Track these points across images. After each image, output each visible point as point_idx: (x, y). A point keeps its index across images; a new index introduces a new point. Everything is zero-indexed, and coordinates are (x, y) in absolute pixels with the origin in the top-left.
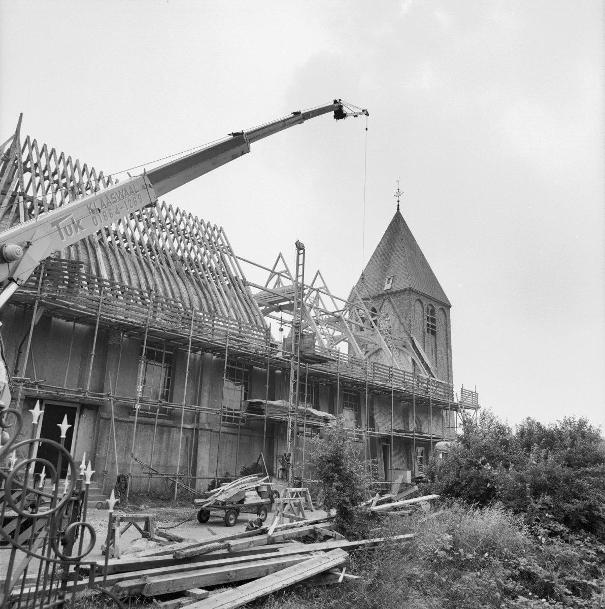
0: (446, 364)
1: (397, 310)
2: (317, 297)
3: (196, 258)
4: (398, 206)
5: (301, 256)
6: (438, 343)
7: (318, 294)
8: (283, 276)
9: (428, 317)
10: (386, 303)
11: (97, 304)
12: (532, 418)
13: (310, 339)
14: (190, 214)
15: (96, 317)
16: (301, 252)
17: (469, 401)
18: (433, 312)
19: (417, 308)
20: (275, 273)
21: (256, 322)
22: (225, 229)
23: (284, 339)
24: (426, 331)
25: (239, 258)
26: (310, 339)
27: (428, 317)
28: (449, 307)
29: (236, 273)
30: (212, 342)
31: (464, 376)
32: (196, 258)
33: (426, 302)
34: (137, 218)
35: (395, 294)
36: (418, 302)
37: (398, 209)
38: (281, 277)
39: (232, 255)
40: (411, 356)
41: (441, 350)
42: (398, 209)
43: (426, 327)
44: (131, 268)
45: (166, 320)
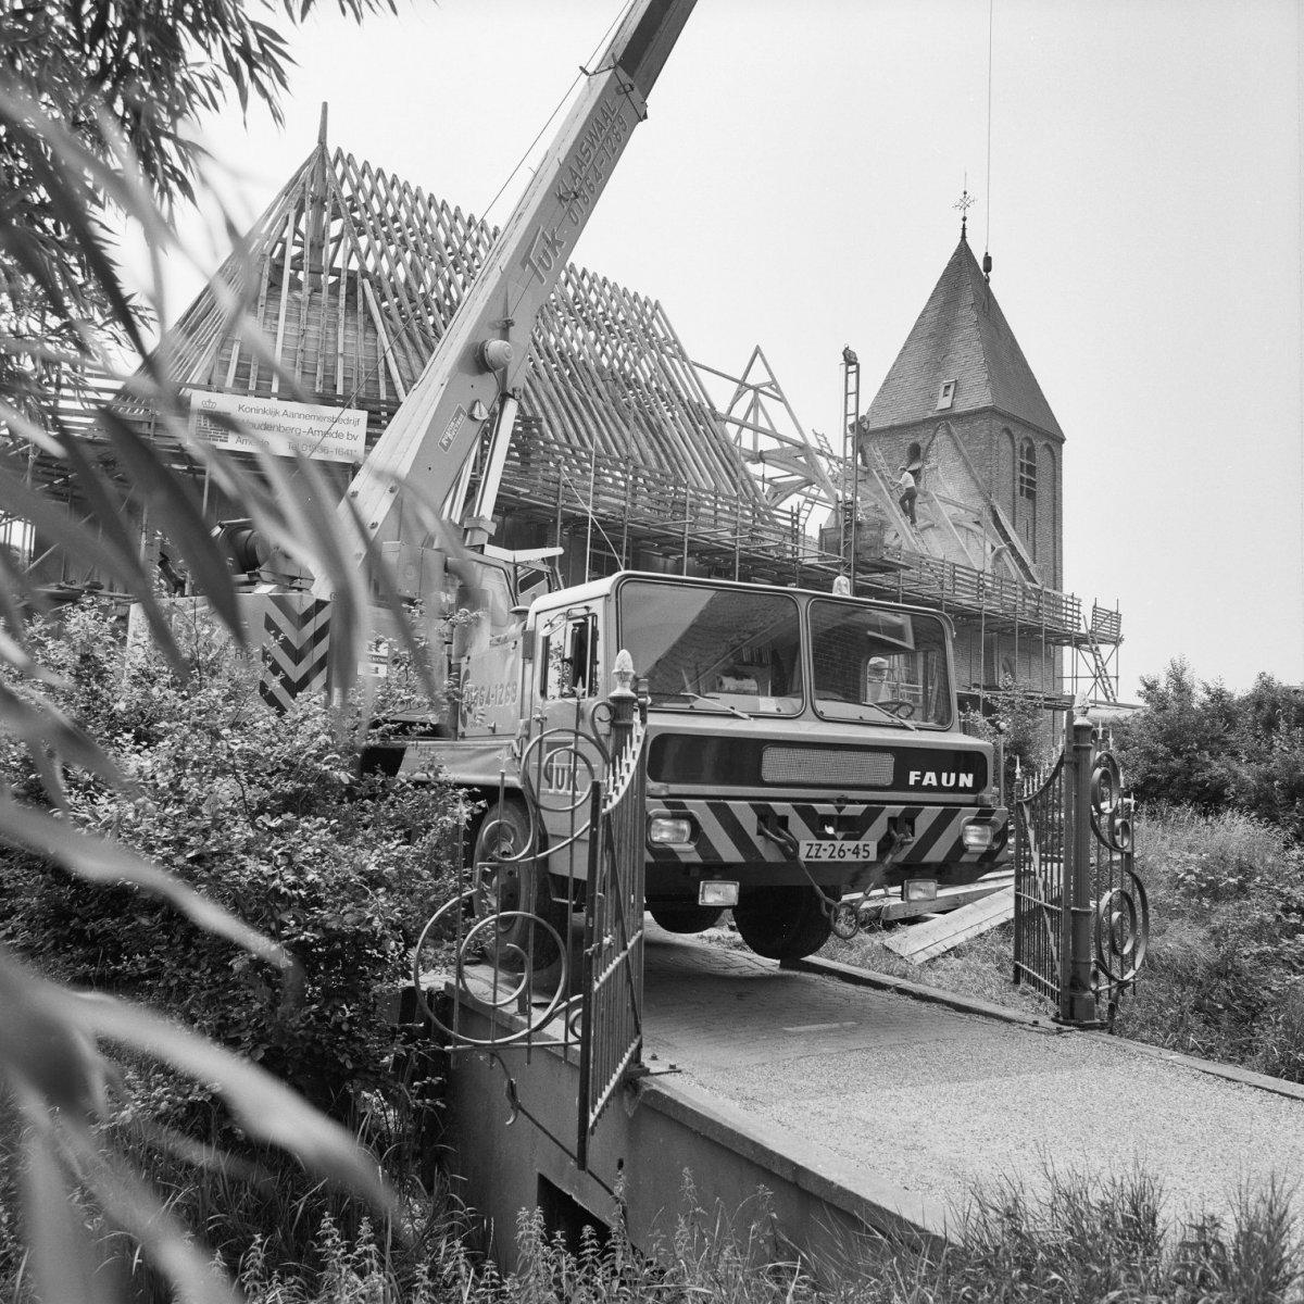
0: (1051, 556)
1: (965, 451)
2: (755, 404)
3: (610, 366)
4: (964, 229)
5: (852, 378)
6: (1038, 516)
7: (756, 399)
8: (763, 392)
9: (1022, 464)
10: (941, 437)
11: (556, 486)
12: (1268, 674)
13: (874, 533)
14: (605, 280)
15: (556, 511)
16: (852, 368)
17: (1104, 630)
18: (1030, 453)
19: (1003, 447)
20: (746, 385)
21: (568, 438)
22: (662, 304)
23: (822, 531)
24: (1018, 492)
25: (701, 367)
26: (874, 533)
27: (1022, 464)
28: (1062, 440)
29: (699, 398)
30: (718, 542)
31: (1088, 574)
32: (622, 367)
33: (1018, 434)
34: (452, 267)
35: (960, 417)
36: (1005, 436)
37: (964, 237)
38: (761, 396)
39: (684, 358)
40: (991, 541)
41: (1044, 527)
42: (964, 237)
43: (1018, 483)
44: (548, 405)
45: (651, 509)
